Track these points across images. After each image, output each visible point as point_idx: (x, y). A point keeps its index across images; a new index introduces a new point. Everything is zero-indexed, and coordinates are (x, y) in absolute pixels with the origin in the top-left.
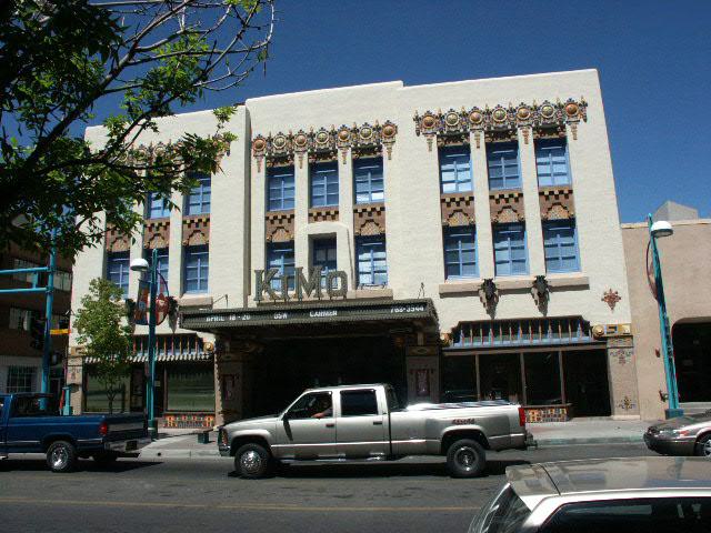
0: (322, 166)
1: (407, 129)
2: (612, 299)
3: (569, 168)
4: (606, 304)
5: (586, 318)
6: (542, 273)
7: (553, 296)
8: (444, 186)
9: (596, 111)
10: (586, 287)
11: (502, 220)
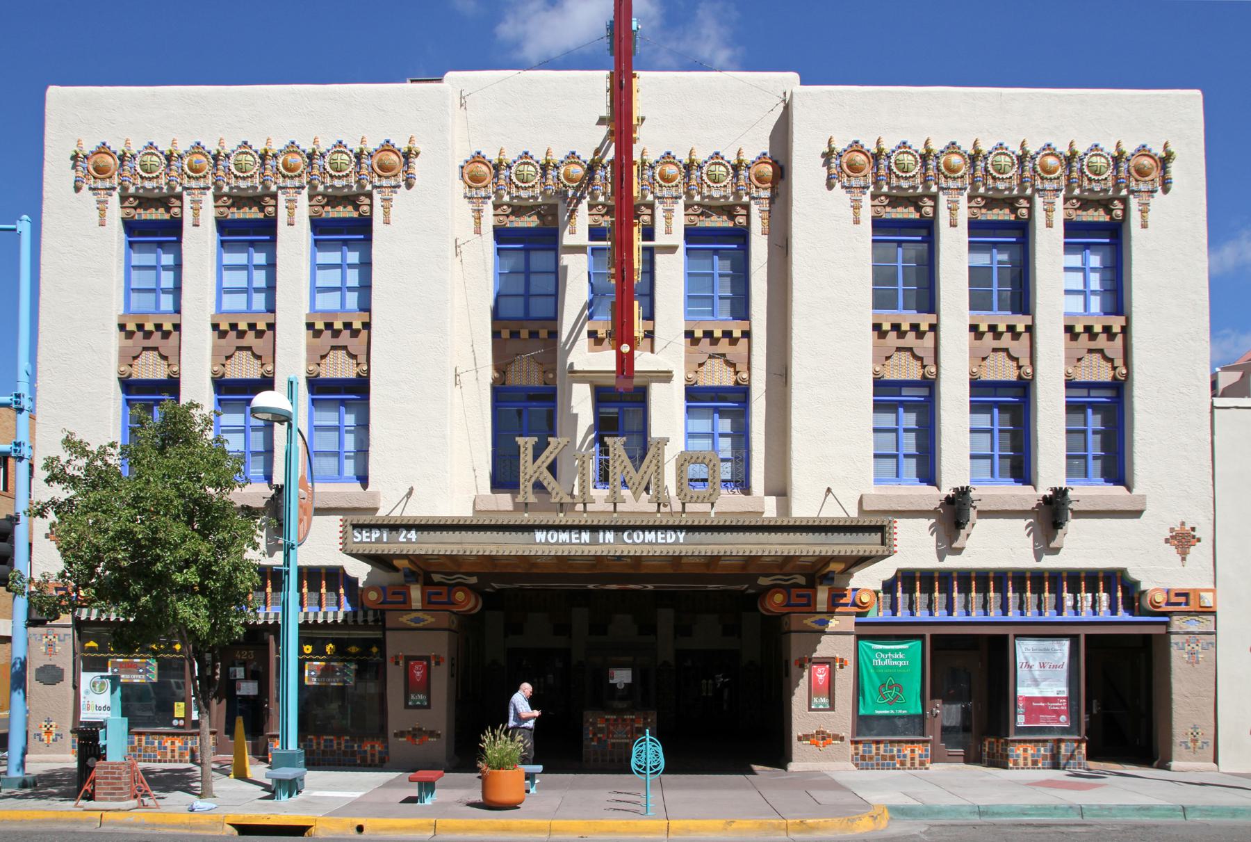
0: (249, 230)
1: (439, 176)
2: (1183, 540)
3: (128, 279)
4: (1172, 550)
5: (1134, 574)
6: (965, 482)
7: (1073, 527)
8: (551, 290)
9: (1190, 173)
10: (1137, 514)
11: (892, 374)
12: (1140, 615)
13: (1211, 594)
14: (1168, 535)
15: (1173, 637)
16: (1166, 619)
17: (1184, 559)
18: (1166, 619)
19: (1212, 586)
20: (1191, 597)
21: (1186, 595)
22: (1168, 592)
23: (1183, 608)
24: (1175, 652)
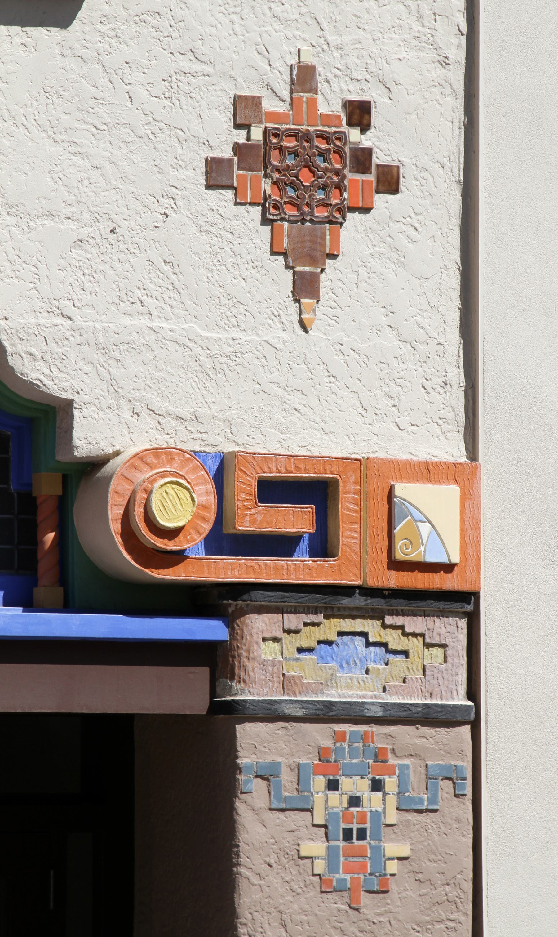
2: (303, 173)
4: (241, 229)
12: (67, 606)
13: (453, 491)
14: (224, 140)
15: (248, 733)
16: (209, 629)
17: (305, 287)
18: (209, 629)
19: (454, 451)
20: (346, 505)
21: (316, 492)
22: (221, 473)
23: (301, 569)
24: (256, 824)
